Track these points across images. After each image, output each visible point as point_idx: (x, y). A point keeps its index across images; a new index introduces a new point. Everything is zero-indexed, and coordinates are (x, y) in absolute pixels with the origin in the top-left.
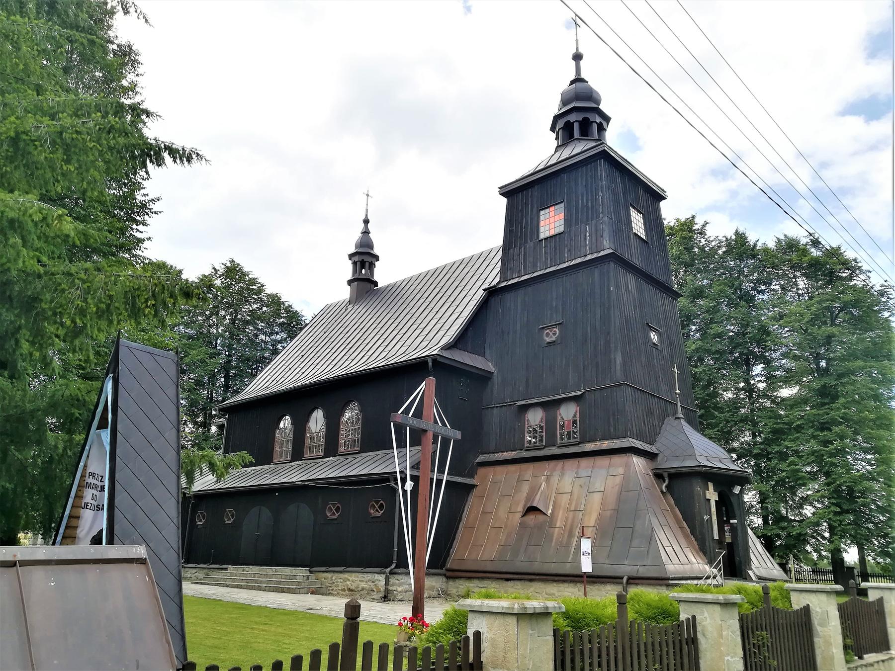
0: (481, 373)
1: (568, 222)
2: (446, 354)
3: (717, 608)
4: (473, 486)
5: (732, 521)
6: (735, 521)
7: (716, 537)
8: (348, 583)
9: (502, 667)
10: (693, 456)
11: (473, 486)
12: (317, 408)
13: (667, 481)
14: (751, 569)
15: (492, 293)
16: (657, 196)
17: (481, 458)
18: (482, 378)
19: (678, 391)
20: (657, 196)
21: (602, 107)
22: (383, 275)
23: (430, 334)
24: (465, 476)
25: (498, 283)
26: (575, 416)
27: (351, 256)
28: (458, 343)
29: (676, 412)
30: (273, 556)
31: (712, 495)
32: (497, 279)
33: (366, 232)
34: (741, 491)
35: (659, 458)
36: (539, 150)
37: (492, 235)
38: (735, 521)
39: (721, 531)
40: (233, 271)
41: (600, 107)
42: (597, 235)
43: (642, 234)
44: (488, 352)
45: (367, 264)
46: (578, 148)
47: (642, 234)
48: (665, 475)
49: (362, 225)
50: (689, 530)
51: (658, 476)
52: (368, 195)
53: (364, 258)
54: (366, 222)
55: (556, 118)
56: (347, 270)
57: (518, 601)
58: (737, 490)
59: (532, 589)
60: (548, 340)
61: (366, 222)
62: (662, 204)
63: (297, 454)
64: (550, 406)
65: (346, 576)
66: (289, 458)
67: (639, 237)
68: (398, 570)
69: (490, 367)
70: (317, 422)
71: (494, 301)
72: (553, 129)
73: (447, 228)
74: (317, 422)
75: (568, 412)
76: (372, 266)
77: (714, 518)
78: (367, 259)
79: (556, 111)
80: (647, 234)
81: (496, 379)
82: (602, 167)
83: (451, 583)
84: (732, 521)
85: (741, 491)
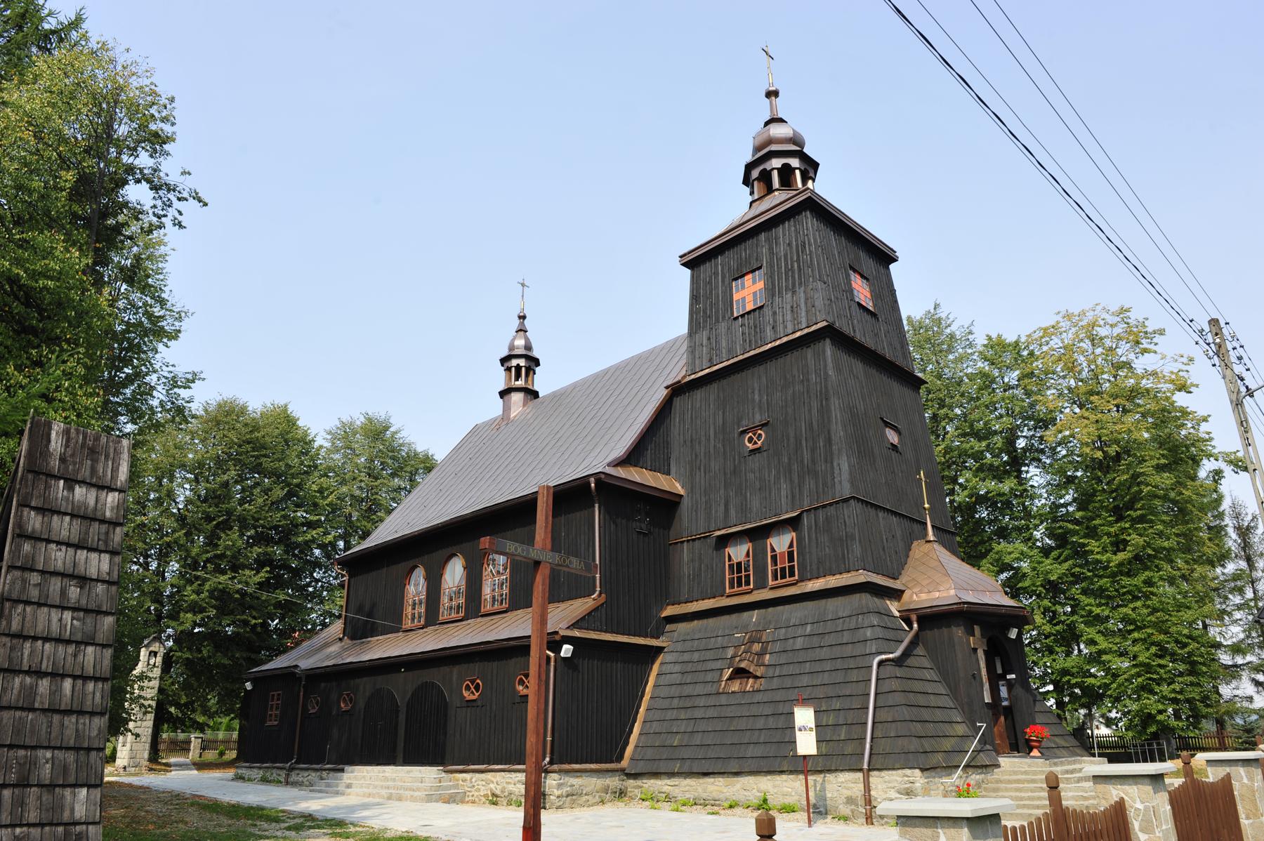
0: (666, 496)
2: (621, 472)
3: (1147, 781)
6: (1013, 676)
7: (987, 699)
8: (492, 786)
12: (454, 555)
15: (677, 390)
16: (885, 257)
17: (669, 611)
18: (666, 505)
19: (927, 506)
20: (885, 257)
22: (543, 382)
23: (596, 453)
24: (646, 636)
25: (684, 377)
26: (791, 545)
27: (503, 361)
28: (632, 457)
29: (926, 534)
32: (683, 373)
33: (522, 330)
34: (1020, 635)
35: (906, 596)
36: (732, 206)
37: (672, 319)
38: (1013, 676)
39: (995, 691)
41: (805, 150)
44: (673, 469)
46: (779, 199)
48: (914, 617)
49: (517, 322)
52: (523, 285)
53: (520, 365)
55: (749, 167)
57: (203, 659)
58: (1013, 634)
59: (738, 786)
60: (750, 446)
62: (892, 266)
63: (432, 618)
64: (758, 534)
65: (489, 776)
66: (422, 622)
67: (863, 276)
68: (555, 767)
69: (679, 488)
70: (454, 573)
71: (677, 402)
72: (747, 181)
73: (623, 322)
74: (454, 573)
75: (781, 543)
76: (530, 371)
79: (749, 158)
80: (875, 306)
81: (686, 504)
82: (808, 222)
83: (631, 782)
85: (1020, 635)
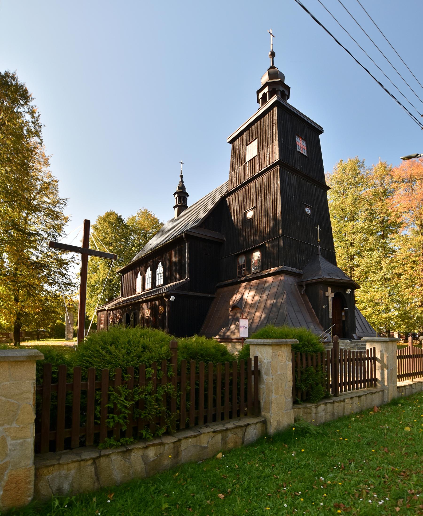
1: (259, 149)
4: (213, 298)
5: (345, 309)
6: (347, 308)
9: (421, 341)
10: (157, 226)
11: (213, 298)
13: (305, 288)
14: (355, 333)
17: (219, 284)
19: (319, 240)
21: (286, 82)
27: (174, 195)
30: (50, 337)
31: (330, 294)
33: (182, 182)
40: (146, 214)
42: (273, 152)
43: (305, 152)
45: (182, 197)
47: (305, 152)
48: (304, 285)
50: (315, 314)
51: (300, 286)
54: (182, 176)
56: (173, 201)
61: (182, 176)
77: (330, 307)
78: (183, 195)
84: (345, 309)
